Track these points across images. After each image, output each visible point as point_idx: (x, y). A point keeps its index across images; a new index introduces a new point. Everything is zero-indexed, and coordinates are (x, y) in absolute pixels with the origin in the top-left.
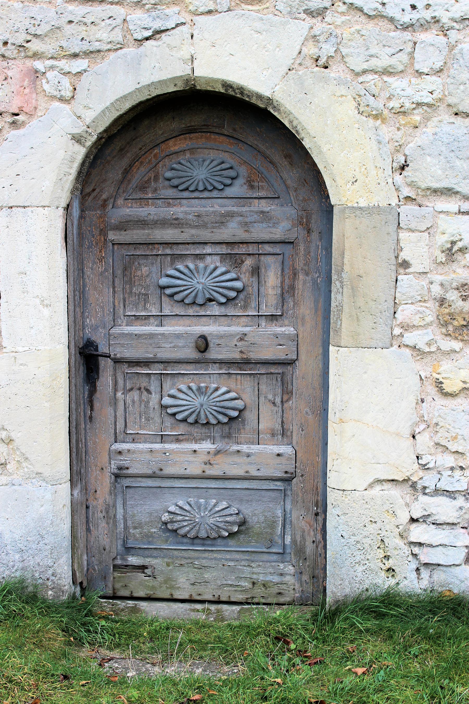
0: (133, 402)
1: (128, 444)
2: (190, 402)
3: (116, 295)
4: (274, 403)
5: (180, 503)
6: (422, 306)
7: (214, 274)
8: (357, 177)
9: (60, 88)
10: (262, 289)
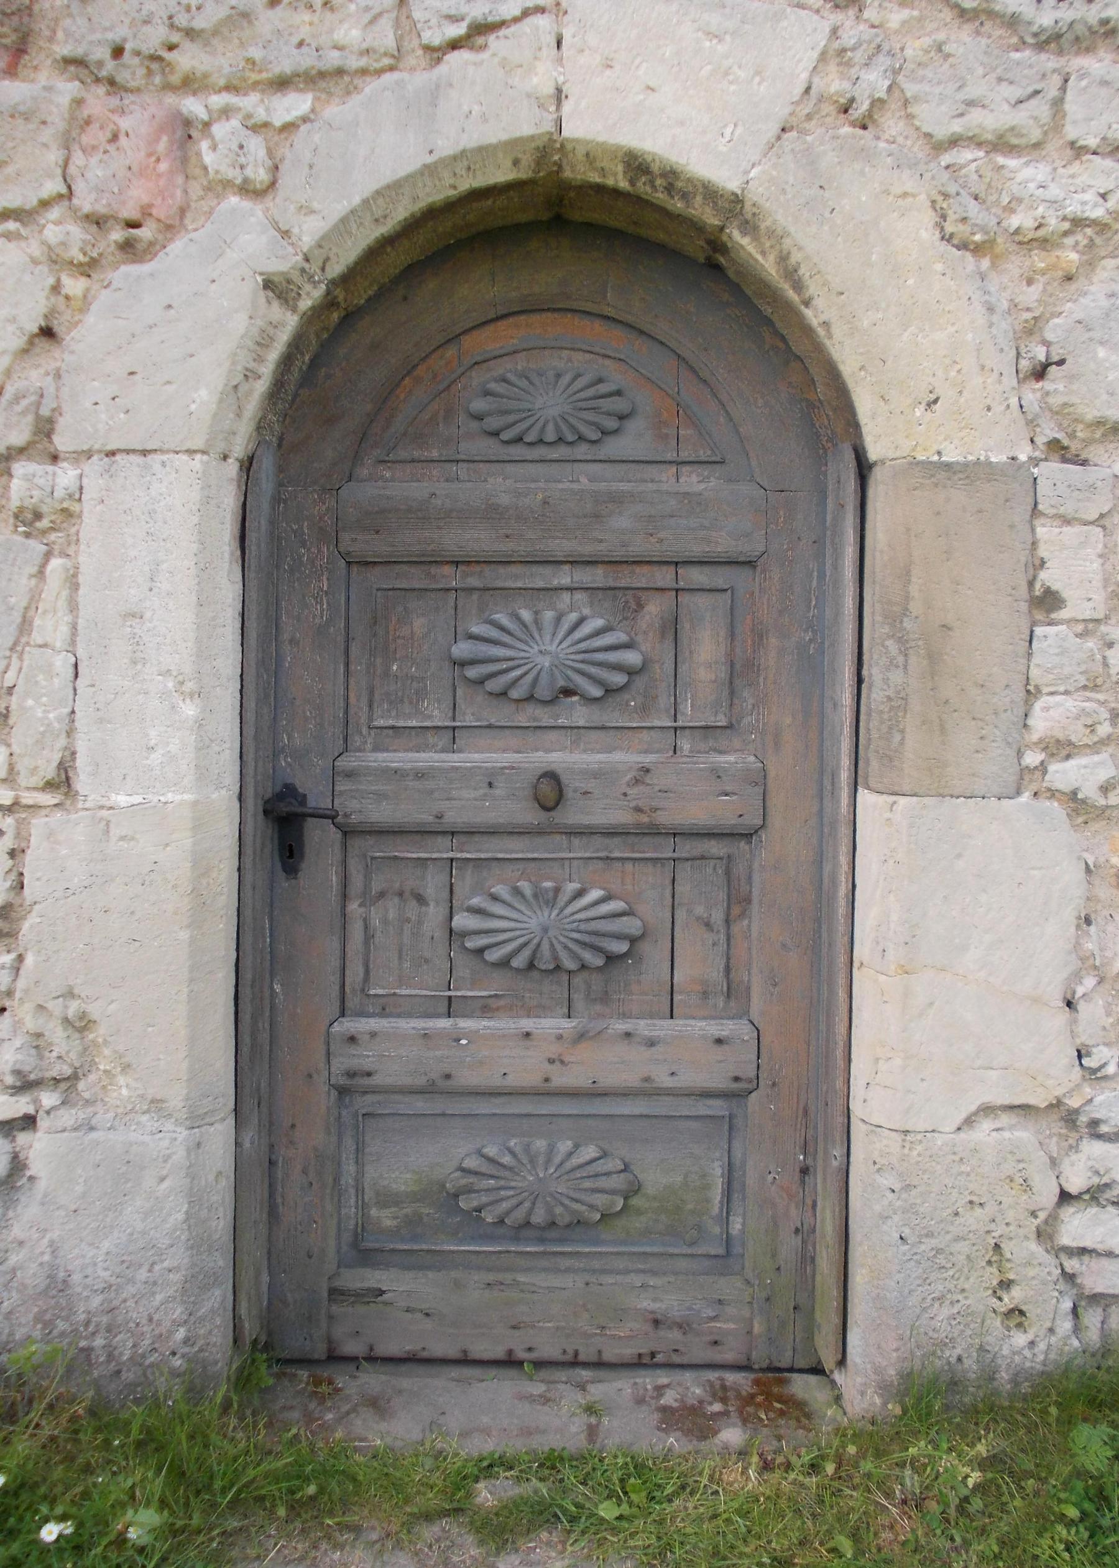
0: (385, 921)
1: (372, 1021)
2: (519, 924)
3: (352, 681)
4: (708, 925)
5: (491, 1151)
6: (1089, 699)
7: (578, 634)
8: (938, 391)
9: (242, 160)
10: (683, 669)
